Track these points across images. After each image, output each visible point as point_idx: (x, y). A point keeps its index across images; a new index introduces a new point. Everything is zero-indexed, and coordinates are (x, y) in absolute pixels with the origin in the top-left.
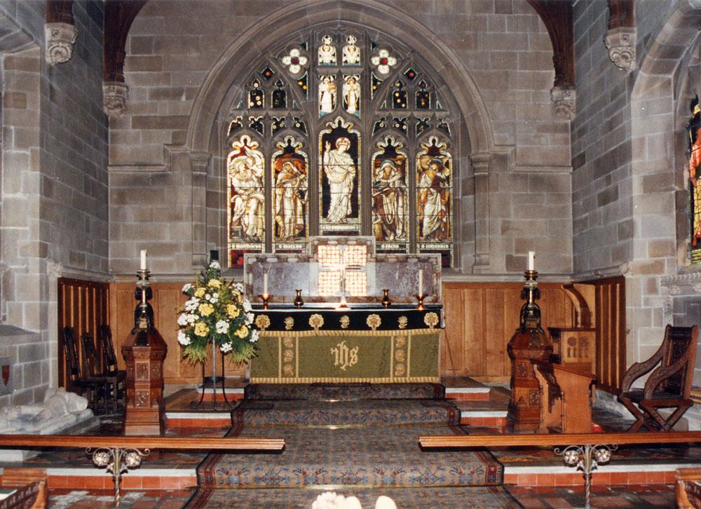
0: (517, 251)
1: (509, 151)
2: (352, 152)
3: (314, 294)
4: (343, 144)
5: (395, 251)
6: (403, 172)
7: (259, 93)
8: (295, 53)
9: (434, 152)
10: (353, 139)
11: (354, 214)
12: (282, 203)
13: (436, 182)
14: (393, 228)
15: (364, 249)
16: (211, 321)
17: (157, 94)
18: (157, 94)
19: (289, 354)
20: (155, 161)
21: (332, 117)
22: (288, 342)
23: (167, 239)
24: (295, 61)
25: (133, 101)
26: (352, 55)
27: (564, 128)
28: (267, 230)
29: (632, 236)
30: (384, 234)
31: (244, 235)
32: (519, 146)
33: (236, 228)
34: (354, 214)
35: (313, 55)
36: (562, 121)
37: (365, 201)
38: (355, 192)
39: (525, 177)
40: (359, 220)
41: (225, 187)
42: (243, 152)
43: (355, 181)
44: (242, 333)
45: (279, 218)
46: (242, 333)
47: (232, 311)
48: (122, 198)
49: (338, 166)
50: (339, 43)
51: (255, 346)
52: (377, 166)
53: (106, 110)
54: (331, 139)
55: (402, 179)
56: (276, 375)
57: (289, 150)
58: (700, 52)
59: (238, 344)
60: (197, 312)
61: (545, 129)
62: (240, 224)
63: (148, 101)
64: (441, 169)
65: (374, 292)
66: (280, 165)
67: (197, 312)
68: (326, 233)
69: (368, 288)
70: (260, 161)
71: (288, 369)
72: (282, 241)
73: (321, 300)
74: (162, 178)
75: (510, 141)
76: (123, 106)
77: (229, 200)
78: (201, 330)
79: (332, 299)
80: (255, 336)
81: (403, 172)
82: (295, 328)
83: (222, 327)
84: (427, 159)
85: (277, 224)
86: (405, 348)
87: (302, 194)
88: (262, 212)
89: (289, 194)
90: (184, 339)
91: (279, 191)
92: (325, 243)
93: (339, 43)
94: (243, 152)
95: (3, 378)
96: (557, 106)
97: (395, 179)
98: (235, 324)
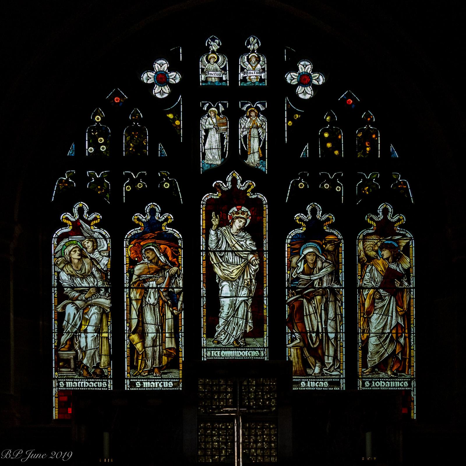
2: (253, 229)
6: (336, 264)
8: (162, 65)
9: (385, 229)
10: (255, 206)
13: (390, 280)
21: (219, 172)
26: (254, 70)
31: (78, 366)
33: (66, 354)
34: (257, 333)
35: (190, 69)
45: (135, 338)
49: (232, 253)
50: (233, 52)
54: (221, 208)
57: (153, 226)
64: (396, 258)
81: (336, 264)
93: (233, 52)
94: (77, 229)
97: (323, 271)
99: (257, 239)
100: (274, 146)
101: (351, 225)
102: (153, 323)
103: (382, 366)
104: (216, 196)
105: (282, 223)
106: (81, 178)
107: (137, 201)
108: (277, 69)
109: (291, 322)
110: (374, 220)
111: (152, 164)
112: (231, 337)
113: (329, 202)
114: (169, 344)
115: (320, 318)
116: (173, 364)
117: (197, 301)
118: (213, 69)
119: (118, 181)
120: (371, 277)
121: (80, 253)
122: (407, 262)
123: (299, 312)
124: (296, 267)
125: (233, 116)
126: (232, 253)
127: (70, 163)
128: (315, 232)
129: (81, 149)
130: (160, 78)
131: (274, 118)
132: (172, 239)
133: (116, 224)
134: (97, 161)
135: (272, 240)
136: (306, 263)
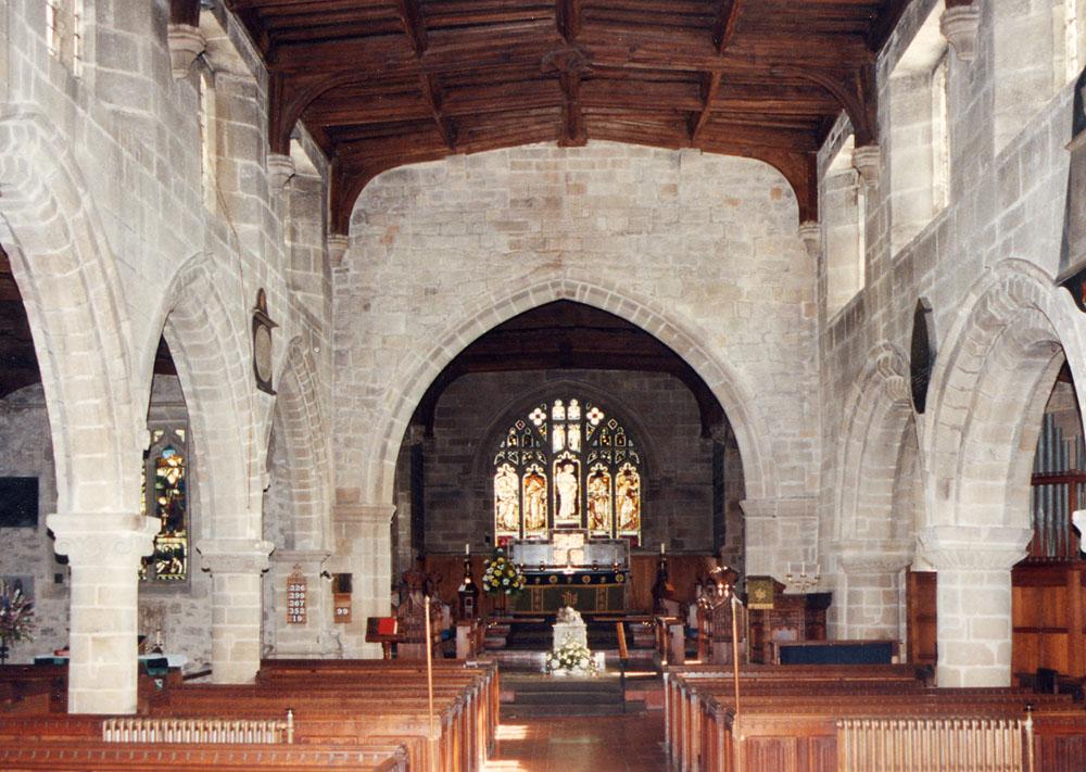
0: (678, 536)
1: (673, 475)
2: (575, 474)
3: (551, 564)
4: (569, 468)
5: (598, 616)
6: (608, 486)
7: (515, 437)
8: (538, 411)
9: (627, 473)
10: (575, 465)
11: (576, 513)
12: (530, 506)
13: (629, 493)
14: (601, 521)
15: (582, 535)
16: (500, 579)
17: (453, 442)
18: (453, 442)
19: (537, 598)
20: (450, 483)
21: (561, 452)
22: (537, 591)
23: (460, 531)
24: (538, 416)
25: (438, 446)
26: (574, 411)
27: (708, 460)
28: (521, 523)
29: (724, 532)
30: (596, 525)
31: (505, 527)
32: (679, 472)
33: (500, 522)
34: (576, 513)
35: (549, 412)
36: (706, 456)
37: (583, 505)
38: (576, 500)
39: (682, 491)
40: (580, 516)
41: (493, 497)
42: (505, 474)
43: (577, 492)
44: (516, 585)
45: (528, 516)
46: (516, 585)
47: (511, 574)
48: (432, 505)
49: (566, 482)
50: (566, 405)
51: (522, 591)
52: (591, 482)
53: (423, 453)
54: (562, 465)
55: (608, 490)
56: (530, 610)
57: (534, 473)
58: (1073, 183)
59: (514, 590)
60: (493, 574)
61: (696, 461)
62: (503, 519)
63: (447, 445)
64: (632, 484)
65: (589, 562)
66: (529, 482)
67: (493, 574)
68: (559, 526)
69: (585, 559)
70: (515, 478)
71: (537, 606)
72: (530, 530)
73: (555, 567)
74: (457, 494)
75: (673, 468)
76: (433, 450)
77: (496, 504)
78: (495, 583)
79: (562, 566)
80: (522, 587)
81: (608, 486)
82: (541, 583)
83: (506, 582)
84: (623, 478)
85: (527, 521)
86: (604, 594)
87: (543, 500)
88: (517, 512)
89: (534, 500)
90: (486, 588)
91: (528, 499)
92: (558, 532)
93: (566, 405)
94: (505, 474)
95: (1032, 484)
96: (704, 449)
97: (603, 488)
98: (512, 580)
99: (576, 476)
100: (583, 442)
101: (614, 470)
103: (627, 526)
104: (560, 461)
105: (586, 470)
106: (506, 455)
107: (529, 462)
108: (584, 412)
109: (590, 509)
110: (622, 470)
113: (605, 462)
114: (542, 518)
115: (602, 508)
116: (543, 525)
117: (552, 502)
118: (558, 411)
119: (520, 455)
120: (621, 492)
121: (505, 483)
122: (637, 486)
123: (592, 506)
124: (591, 488)
125: (566, 430)
126: (566, 482)
127: (502, 449)
128: (599, 474)
129: (506, 443)
130: (537, 417)
132: (542, 478)
133: (520, 471)
135: (582, 474)
136: (596, 487)
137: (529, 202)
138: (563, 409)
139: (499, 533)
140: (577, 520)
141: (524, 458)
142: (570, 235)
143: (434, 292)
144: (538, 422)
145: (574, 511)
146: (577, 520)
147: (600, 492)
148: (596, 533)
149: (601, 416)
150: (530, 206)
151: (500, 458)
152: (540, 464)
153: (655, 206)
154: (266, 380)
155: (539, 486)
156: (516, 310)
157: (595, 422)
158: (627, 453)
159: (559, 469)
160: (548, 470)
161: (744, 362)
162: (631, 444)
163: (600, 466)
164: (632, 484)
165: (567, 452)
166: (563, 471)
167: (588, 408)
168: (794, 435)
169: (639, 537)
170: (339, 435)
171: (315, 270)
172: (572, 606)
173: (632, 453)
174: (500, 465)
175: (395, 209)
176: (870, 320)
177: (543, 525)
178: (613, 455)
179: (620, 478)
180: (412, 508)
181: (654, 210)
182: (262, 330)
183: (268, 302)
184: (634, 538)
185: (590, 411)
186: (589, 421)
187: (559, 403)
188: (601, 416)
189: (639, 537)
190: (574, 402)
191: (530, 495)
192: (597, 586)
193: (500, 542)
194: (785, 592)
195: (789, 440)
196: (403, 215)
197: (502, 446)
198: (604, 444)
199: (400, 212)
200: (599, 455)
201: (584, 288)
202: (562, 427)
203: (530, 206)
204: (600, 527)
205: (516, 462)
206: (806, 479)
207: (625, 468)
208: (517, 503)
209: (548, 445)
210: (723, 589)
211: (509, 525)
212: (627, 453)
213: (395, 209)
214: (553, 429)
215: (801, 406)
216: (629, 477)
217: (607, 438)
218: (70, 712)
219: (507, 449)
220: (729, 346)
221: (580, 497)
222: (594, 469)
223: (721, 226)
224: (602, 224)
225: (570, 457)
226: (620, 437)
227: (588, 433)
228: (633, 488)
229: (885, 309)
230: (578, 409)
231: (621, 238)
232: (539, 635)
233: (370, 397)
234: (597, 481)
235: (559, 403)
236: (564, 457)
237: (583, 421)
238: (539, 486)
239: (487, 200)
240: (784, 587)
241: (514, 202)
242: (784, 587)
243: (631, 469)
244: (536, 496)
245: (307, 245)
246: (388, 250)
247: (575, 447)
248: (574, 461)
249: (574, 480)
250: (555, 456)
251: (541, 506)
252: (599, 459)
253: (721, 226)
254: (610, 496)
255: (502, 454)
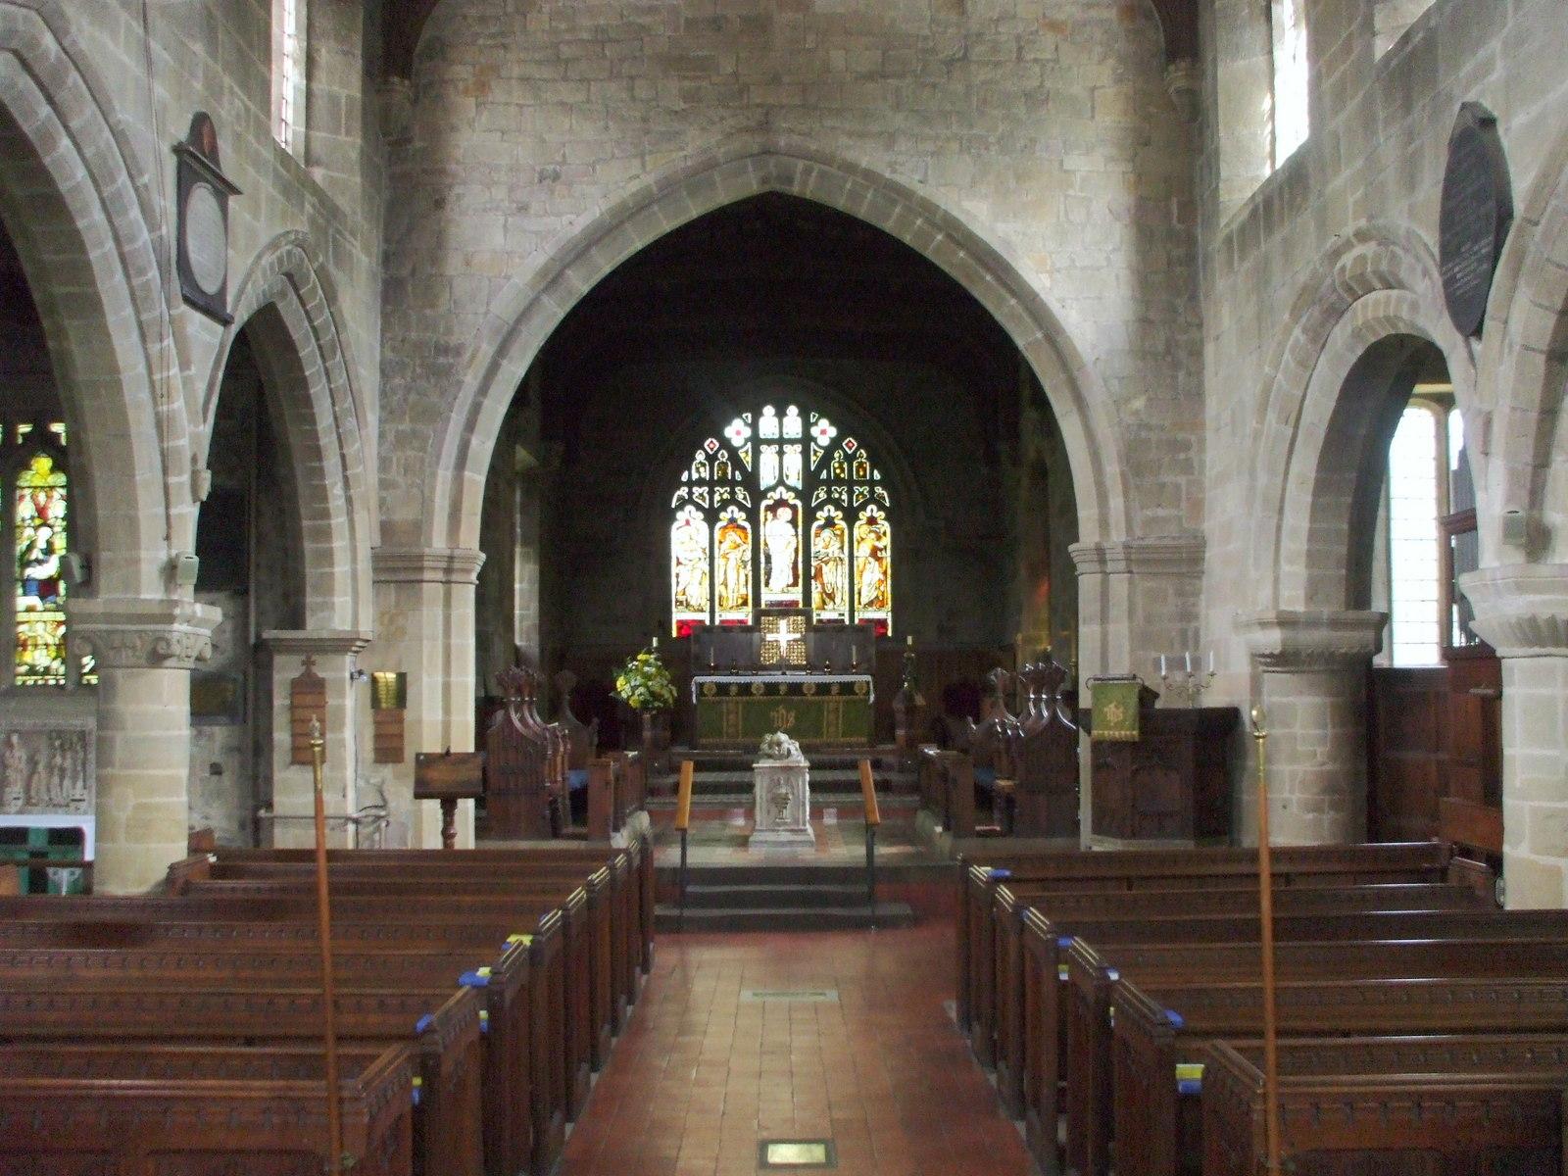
2: (793, 522)
4: (785, 513)
7: (704, 465)
9: (872, 521)
10: (794, 508)
11: (795, 584)
13: (875, 553)
21: (773, 489)
26: (793, 423)
28: (712, 600)
33: (681, 598)
34: (795, 584)
35: (754, 426)
37: (806, 572)
38: (795, 564)
42: (688, 523)
43: (796, 550)
49: (779, 535)
50: (781, 414)
54: (773, 509)
55: (842, 548)
57: (732, 520)
64: (879, 538)
66: (724, 535)
70: (705, 527)
81: (842, 542)
84: (866, 528)
89: (732, 564)
93: (781, 414)
94: (688, 523)
97: (834, 549)
99: (795, 526)
101: (851, 516)
102: (734, 581)
103: (871, 603)
104: (771, 502)
105: (810, 516)
106: (690, 493)
107: (725, 505)
108: (807, 425)
109: (815, 578)
110: (864, 516)
111: (733, 483)
112: (779, 587)
113: (838, 504)
114: (743, 591)
115: (834, 576)
116: (745, 603)
117: (759, 565)
119: (711, 493)
120: (863, 551)
121: (687, 535)
122: (886, 541)
123: (819, 571)
124: (818, 545)
125: (781, 453)
128: (830, 523)
130: (737, 431)
131: (806, 454)
133: (711, 516)
134: (701, 482)
136: (825, 543)
137: (716, 23)
138: (776, 420)
139: (678, 615)
140: (796, 594)
141: (717, 497)
142: (786, 79)
143: (556, 177)
144: (737, 442)
145: (791, 581)
146: (796, 594)
147: (830, 551)
148: (826, 615)
149: (833, 432)
150: (719, 29)
151: (680, 498)
152: (742, 507)
153: (927, 32)
154: (210, 287)
155: (739, 541)
156: (694, 210)
157: (824, 441)
158: (872, 492)
159: (770, 515)
160: (753, 516)
161: (1077, 299)
162: (877, 476)
163: (830, 510)
164: (879, 538)
165: (781, 489)
166: (775, 516)
167: (812, 420)
168: (1162, 428)
169: (890, 622)
170: (387, 427)
171: (348, 133)
172: (785, 732)
173: (879, 490)
174: (680, 507)
175: (492, 36)
176: (1321, 194)
177: (745, 603)
178: (850, 493)
179: (861, 529)
180: (542, 573)
181: (926, 38)
182: (202, 198)
183: (220, 143)
184: (882, 623)
185: (816, 424)
186: (815, 440)
187: (769, 411)
188: (833, 432)
189: (890, 622)
190: (793, 410)
191: (725, 556)
192: (826, 698)
193: (680, 628)
194: (1159, 705)
195: (1154, 436)
196: (505, 47)
197: (685, 477)
198: (837, 476)
199: (500, 40)
200: (829, 492)
201: (808, 171)
202: (775, 448)
203: (719, 29)
204: (830, 605)
205: (706, 506)
206: (1184, 504)
207: (868, 513)
208: (707, 569)
209: (751, 481)
210: (1037, 702)
211: (693, 602)
212: (872, 492)
213: (492, 36)
214: (760, 452)
215: (1174, 378)
216: (873, 528)
217: (841, 464)
218: (439, 801)
219: (690, 484)
220: (1051, 273)
221: (800, 559)
222: (821, 515)
223: (1037, 69)
224: (838, 59)
225: (785, 497)
226: (861, 465)
227: (813, 458)
228: (880, 545)
229: (1359, 163)
230: (799, 420)
231: (870, 86)
232: (735, 777)
233: (441, 360)
234: (827, 533)
235: (769, 411)
236: (776, 495)
237: (806, 440)
238: (739, 541)
239: (646, 20)
240: (1156, 695)
241: (691, 24)
242: (1156, 695)
243: (876, 514)
244: (735, 555)
245: (336, 88)
246: (478, 106)
247: (795, 479)
248: (791, 502)
249: (793, 532)
250: (763, 495)
251: (742, 573)
252: (829, 500)
253: (1037, 69)
254: (846, 557)
255: (683, 491)
